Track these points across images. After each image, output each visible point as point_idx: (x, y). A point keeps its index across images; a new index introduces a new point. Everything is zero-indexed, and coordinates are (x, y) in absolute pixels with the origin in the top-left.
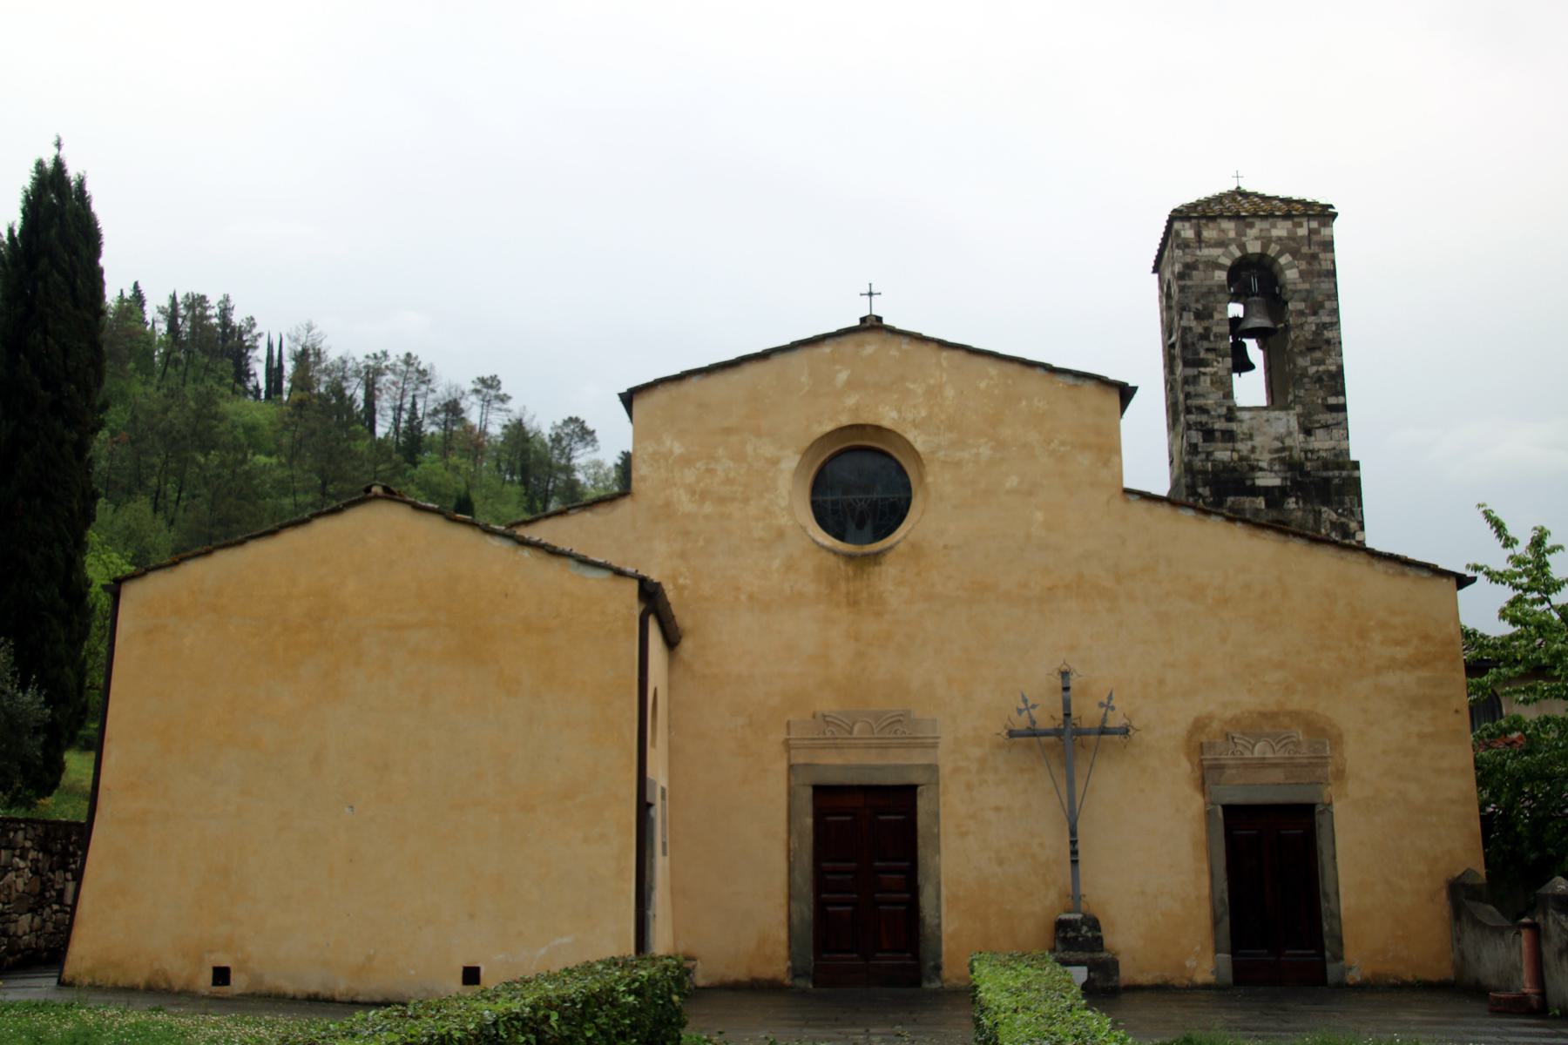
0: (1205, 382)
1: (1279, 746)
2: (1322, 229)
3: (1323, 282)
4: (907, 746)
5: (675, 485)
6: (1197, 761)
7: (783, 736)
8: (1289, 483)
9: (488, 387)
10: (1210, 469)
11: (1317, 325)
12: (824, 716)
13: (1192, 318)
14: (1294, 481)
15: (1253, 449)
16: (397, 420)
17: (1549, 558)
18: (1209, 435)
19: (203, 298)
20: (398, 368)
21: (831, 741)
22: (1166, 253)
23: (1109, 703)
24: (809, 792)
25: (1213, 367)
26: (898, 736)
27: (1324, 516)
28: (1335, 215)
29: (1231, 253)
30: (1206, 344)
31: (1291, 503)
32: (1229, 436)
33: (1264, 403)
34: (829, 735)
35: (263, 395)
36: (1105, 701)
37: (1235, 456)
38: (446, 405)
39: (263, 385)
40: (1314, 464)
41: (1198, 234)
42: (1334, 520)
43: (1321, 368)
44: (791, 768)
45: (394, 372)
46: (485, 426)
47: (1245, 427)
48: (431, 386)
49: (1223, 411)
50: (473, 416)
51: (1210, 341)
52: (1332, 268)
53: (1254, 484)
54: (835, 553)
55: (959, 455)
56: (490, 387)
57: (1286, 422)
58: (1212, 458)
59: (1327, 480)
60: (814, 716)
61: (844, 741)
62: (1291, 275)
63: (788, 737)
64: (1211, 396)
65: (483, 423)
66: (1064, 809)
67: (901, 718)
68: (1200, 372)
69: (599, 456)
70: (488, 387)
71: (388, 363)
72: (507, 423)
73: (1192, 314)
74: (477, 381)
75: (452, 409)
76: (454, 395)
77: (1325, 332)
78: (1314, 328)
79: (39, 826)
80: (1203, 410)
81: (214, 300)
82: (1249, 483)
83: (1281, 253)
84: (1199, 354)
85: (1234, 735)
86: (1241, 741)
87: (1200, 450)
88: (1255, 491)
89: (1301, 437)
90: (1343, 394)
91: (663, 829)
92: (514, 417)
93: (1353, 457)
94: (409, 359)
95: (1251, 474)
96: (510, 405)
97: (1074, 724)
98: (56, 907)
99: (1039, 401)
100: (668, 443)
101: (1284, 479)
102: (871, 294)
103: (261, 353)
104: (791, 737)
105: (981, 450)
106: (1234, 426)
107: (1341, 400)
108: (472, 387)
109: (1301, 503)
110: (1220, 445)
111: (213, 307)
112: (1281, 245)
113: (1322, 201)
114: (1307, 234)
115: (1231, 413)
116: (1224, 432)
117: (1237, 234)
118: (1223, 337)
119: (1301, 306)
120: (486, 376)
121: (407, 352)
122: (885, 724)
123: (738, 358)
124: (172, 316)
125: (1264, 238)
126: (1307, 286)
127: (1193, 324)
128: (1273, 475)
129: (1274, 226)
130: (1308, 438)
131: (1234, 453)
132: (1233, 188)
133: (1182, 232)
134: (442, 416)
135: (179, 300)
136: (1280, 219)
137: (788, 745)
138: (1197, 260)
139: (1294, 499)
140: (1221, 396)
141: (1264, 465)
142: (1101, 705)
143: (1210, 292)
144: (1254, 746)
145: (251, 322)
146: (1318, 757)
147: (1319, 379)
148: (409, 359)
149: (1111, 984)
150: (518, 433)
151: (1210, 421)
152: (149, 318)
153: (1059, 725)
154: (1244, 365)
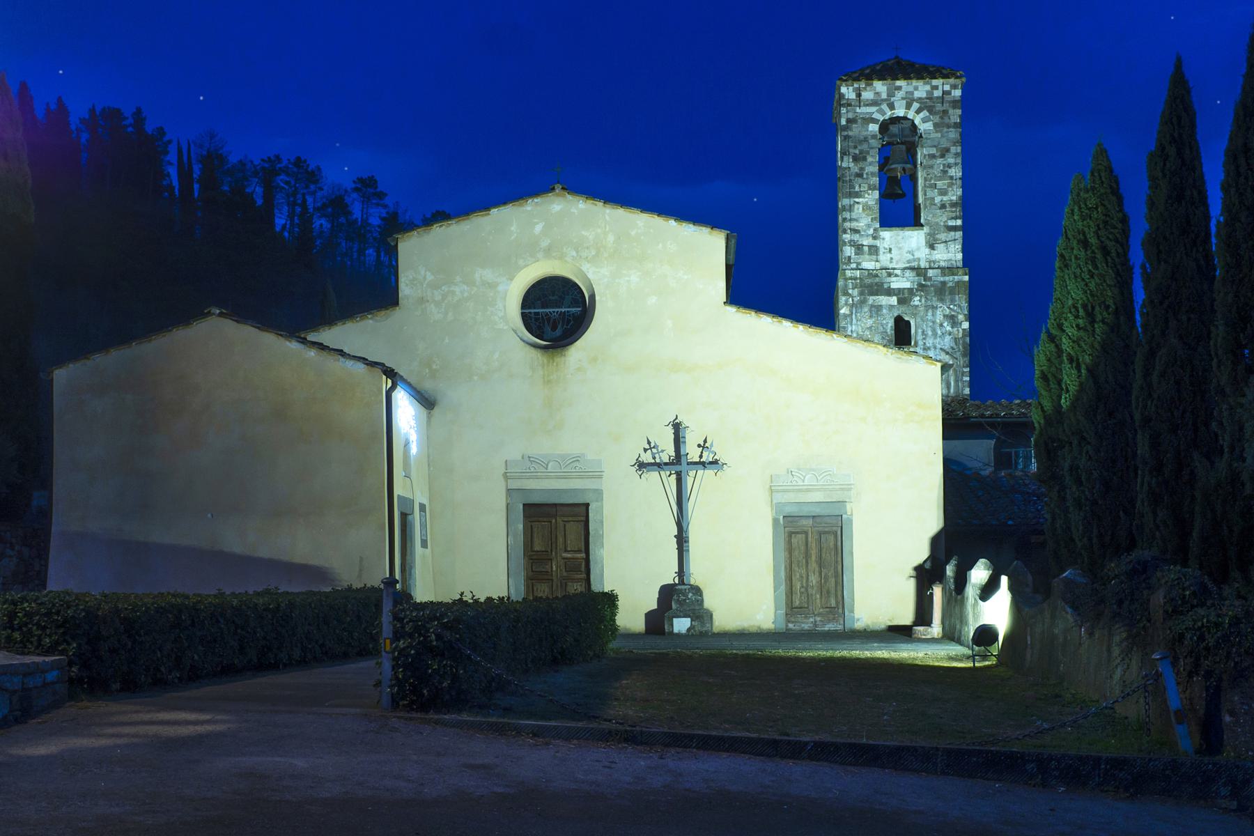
0: (858, 209)
1: (821, 477)
2: (953, 91)
4: (581, 477)
5: (428, 301)
6: (768, 487)
7: (503, 470)
8: (916, 287)
10: (858, 276)
11: (944, 165)
12: (529, 457)
13: (851, 160)
18: (859, 248)
21: (535, 474)
23: (704, 445)
24: (521, 507)
25: (864, 198)
34: (532, 470)
36: (702, 444)
41: (859, 95)
42: (947, 313)
43: (945, 198)
44: (508, 490)
46: (367, 219)
48: (318, 185)
50: (357, 211)
59: (944, 283)
60: (523, 458)
61: (542, 474)
65: (365, 216)
68: (855, 202)
74: (357, 181)
77: (950, 171)
80: (856, 231)
82: (886, 286)
84: (855, 188)
86: (797, 474)
87: (852, 261)
89: (927, 250)
95: (888, 279)
96: (387, 201)
99: (671, 245)
103: (172, 156)
106: (877, 243)
108: (354, 186)
109: (923, 300)
111: (127, 118)
112: (920, 103)
114: (941, 95)
116: (870, 247)
117: (888, 95)
125: (908, 98)
127: (852, 165)
130: (932, 251)
131: (877, 263)
138: (857, 116)
139: (918, 298)
140: (870, 220)
142: (699, 446)
143: (866, 140)
144: (804, 477)
145: (161, 131)
148: (299, 162)
149: (704, 629)
151: (860, 240)
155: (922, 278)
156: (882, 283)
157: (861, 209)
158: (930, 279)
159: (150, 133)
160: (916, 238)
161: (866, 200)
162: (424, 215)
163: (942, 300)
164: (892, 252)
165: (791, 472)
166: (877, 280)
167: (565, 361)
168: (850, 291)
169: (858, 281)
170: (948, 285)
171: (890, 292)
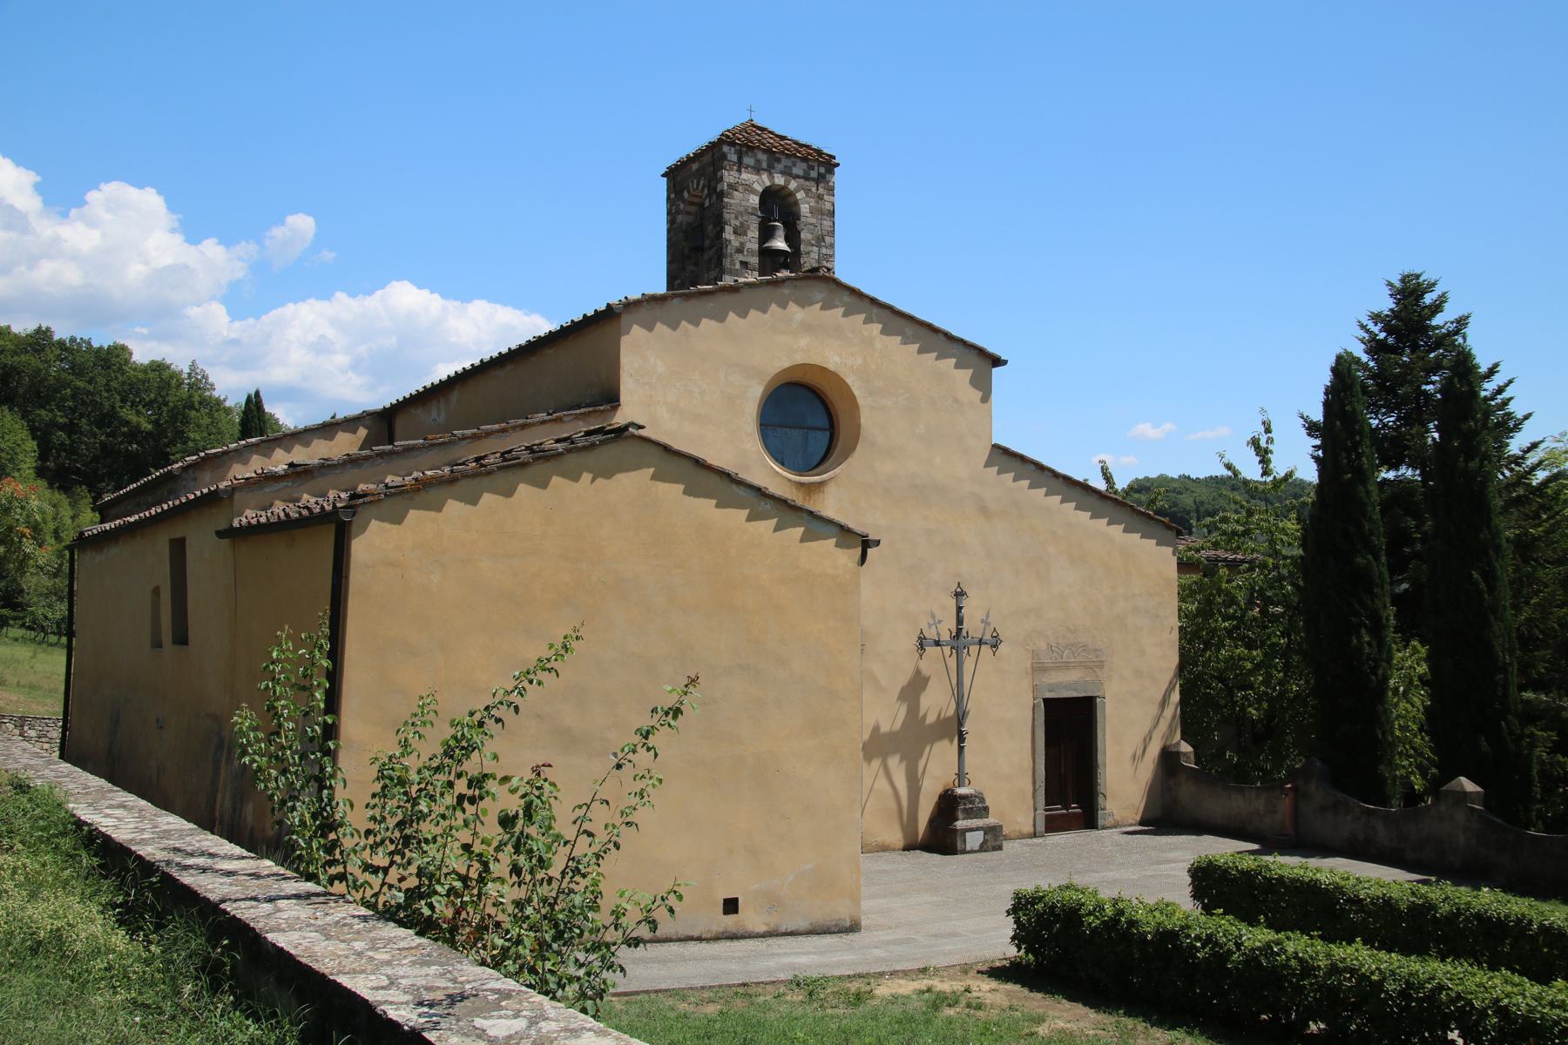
17: (1121, 484)
30: (741, 257)
36: (985, 618)
51: (744, 256)
54: (790, 480)
62: (804, 209)
66: (252, 858)
83: (797, 190)
118: (751, 252)
119: (809, 236)
126: (813, 221)
127: (732, 237)
132: (745, 119)
133: (729, 155)
144: (1063, 652)
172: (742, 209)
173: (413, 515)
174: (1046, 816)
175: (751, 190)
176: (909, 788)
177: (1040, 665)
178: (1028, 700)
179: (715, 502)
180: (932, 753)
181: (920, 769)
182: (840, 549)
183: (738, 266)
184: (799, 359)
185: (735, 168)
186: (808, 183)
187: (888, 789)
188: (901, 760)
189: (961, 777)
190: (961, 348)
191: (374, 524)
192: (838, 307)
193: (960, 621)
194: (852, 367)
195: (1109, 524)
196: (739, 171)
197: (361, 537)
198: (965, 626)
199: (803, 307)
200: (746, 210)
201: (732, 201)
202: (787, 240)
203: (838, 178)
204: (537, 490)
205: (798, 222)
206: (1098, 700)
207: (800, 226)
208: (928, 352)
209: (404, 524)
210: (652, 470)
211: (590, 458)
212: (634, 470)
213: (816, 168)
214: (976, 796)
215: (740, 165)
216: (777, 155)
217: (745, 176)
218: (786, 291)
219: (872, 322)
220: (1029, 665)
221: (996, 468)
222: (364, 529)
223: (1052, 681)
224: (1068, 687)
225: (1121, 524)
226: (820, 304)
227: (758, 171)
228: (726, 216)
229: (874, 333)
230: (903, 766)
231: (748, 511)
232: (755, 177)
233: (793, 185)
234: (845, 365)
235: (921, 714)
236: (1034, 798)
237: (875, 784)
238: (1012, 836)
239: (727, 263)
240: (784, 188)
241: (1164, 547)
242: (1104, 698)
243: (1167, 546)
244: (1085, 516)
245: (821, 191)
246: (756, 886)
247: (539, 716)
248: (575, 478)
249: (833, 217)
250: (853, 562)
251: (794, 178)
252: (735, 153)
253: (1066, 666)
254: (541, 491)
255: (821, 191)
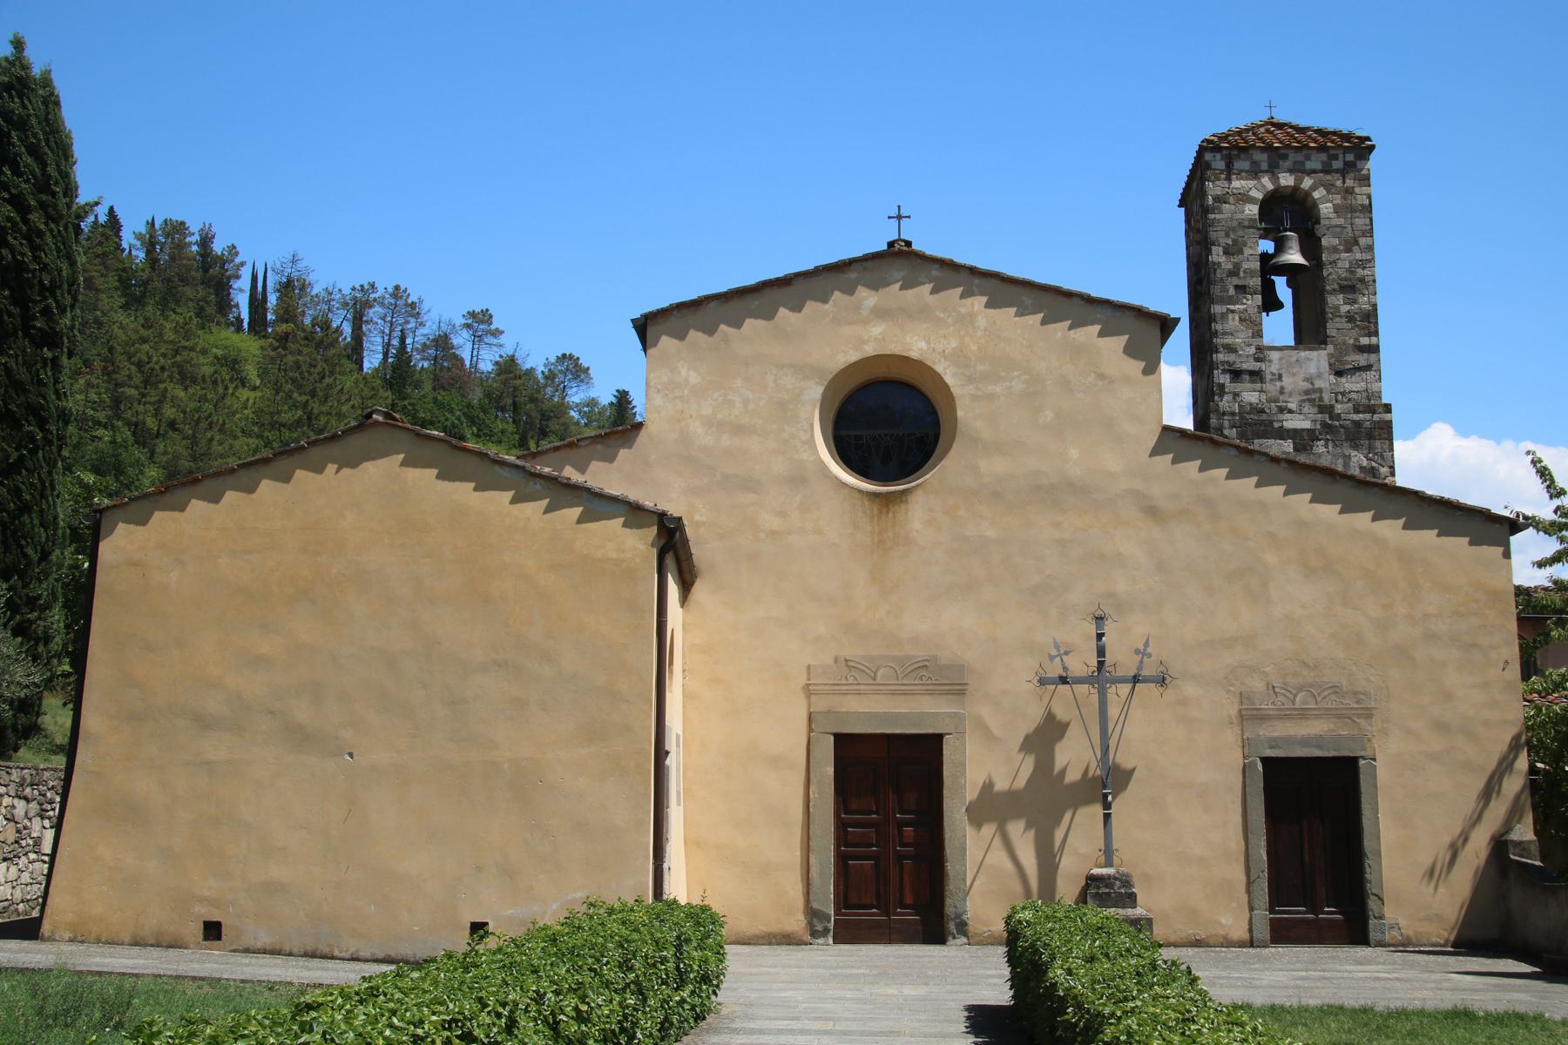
3: (1358, 217)
7: (805, 681)
8: (1319, 427)
9: (480, 322)
10: (1237, 411)
11: (1350, 262)
12: (846, 660)
14: (1324, 425)
15: (1282, 390)
16: (386, 355)
19: (183, 223)
20: (386, 302)
22: (1195, 185)
23: (1145, 650)
26: (924, 682)
27: (1353, 459)
28: (1372, 148)
29: (1264, 186)
30: (1235, 281)
31: (1320, 447)
32: (1256, 375)
33: (1292, 343)
34: (851, 680)
35: (246, 325)
36: (1142, 647)
37: (1264, 397)
38: (436, 340)
39: (245, 315)
40: (1345, 406)
45: (382, 305)
47: (1274, 368)
49: (1252, 350)
51: (1240, 278)
52: (1368, 203)
53: (1282, 427)
55: (991, 388)
56: (482, 322)
57: (1316, 361)
58: (1239, 399)
59: (1358, 424)
60: (836, 660)
62: (1326, 209)
63: (808, 682)
64: (1240, 335)
65: (475, 359)
67: (928, 664)
68: (1228, 309)
69: (593, 393)
70: (480, 322)
71: (376, 295)
72: (498, 359)
73: (1221, 249)
75: (442, 343)
76: (444, 327)
78: (1347, 266)
79: (13, 770)
80: (1231, 349)
81: (194, 227)
82: (1276, 425)
83: (1314, 188)
85: (1275, 685)
86: (1283, 691)
88: (1283, 434)
89: (1332, 378)
90: (1376, 334)
91: (678, 777)
92: (508, 350)
93: (1385, 400)
94: (397, 292)
95: (1281, 417)
96: (503, 339)
97: (1109, 672)
98: (32, 856)
100: (684, 372)
101: (1314, 421)
102: (899, 217)
103: (244, 283)
104: (811, 682)
105: (1014, 384)
107: (1374, 340)
108: (463, 321)
110: (1249, 385)
111: (193, 234)
113: (1359, 133)
115: (1261, 353)
118: (1251, 273)
120: (478, 310)
121: (395, 284)
122: (909, 670)
123: (758, 284)
124: (150, 244)
126: (1341, 221)
127: (1222, 259)
128: (1302, 417)
129: (1308, 158)
132: (1265, 117)
133: (1213, 163)
134: (432, 352)
135: (157, 226)
136: (1315, 151)
137: (808, 691)
141: (1292, 406)
142: (1137, 651)
144: (1295, 696)
146: (1362, 708)
147: (1350, 318)
148: (397, 292)
150: (508, 367)
151: (1238, 361)
152: (125, 245)
153: (1093, 672)
154: (1271, 303)
155: (1327, 416)
156: (1271, 422)
157: (1237, 318)
158: (1338, 417)
159: (220, 254)
160: (1315, 360)
161: (1245, 306)
162: (547, 359)
163: (1356, 447)
164: (1283, 379)
165: (1273, 687)
166: (1264, 417)
167: (906, 509)
168: (1226, 432)
169: (1237, 418)
170: (1364, 426)
171: (1283, 434)
172: (1235, 224)
173: (158, 516)
174: (1271, 919)
175: (1248, 199)
176: (1041, 866)
177: (1255, 713)
178: (1236, 759)
179: (473, 485)
180: (1075, 820)
181: (1057, 843)
182: (629, 530)
183: (1232, 291)
184: (870, 350)
185: (1223, 176)
186: (1329, 177)
187: (1008, 865)
188: (1027, 827)
189: (1108, 854)
190: (1108, 312)
191: (121, 525)
192: (924, 284)
193: (1101, 652)
194: (944, 351)
195: (1374, 519)
196: (1229, 179)
197: (108, 539)
198: (1109, 659)
199: (876, 289)
200: (1240, 224)
201: (1218, 216)
202: (1304, 254)
203: (1374, 164)
204: (280, 484)
205: (1317, 226)
206: (1362, 762)
207: (1319, 230)
208: (1055, 322)
209: (149, 525)
210: (402, 456)
211: (335, 449)
212: (382, 457)
213: (1341, 156)
214: (1116, 879)
215: (1229, 172)
216: (1282, 151)
217: (1236, 184)
218: (853, 275)
219: (973, 295)
220: (1234, 712)
221: (1171, 456)
222: (111, 532)
223: (1275, 734)
224: (1305, 741)
225: (1399, 518)
226: (901, 283)
227: (1256, 174)
228: (1213, 235)
229: (976, 309)
230: (1031, 834)
231: (513, 492)
232: (1251, 183)
233: (1307, 183)
234: (934, 350)
235: (1057, 768)
236: (1249, 891)
237: (986, 859)
238: (1211, 942)
239: (1216, 290)
240: (1296, 189)
241: (1485, 547)
242: (1374, 760)
243: (1490, 544)
244: (1329, 512)
245: (1349, 183)
246: (510, 911)
247: (271, 713)
248: (319, 470)
249: (1371, 212)
250: (645, 544)
251: (1308, 174)
252: (1222, 160)
253: (1303, 715)
254: (285, 485)
255: (1349, 183)
